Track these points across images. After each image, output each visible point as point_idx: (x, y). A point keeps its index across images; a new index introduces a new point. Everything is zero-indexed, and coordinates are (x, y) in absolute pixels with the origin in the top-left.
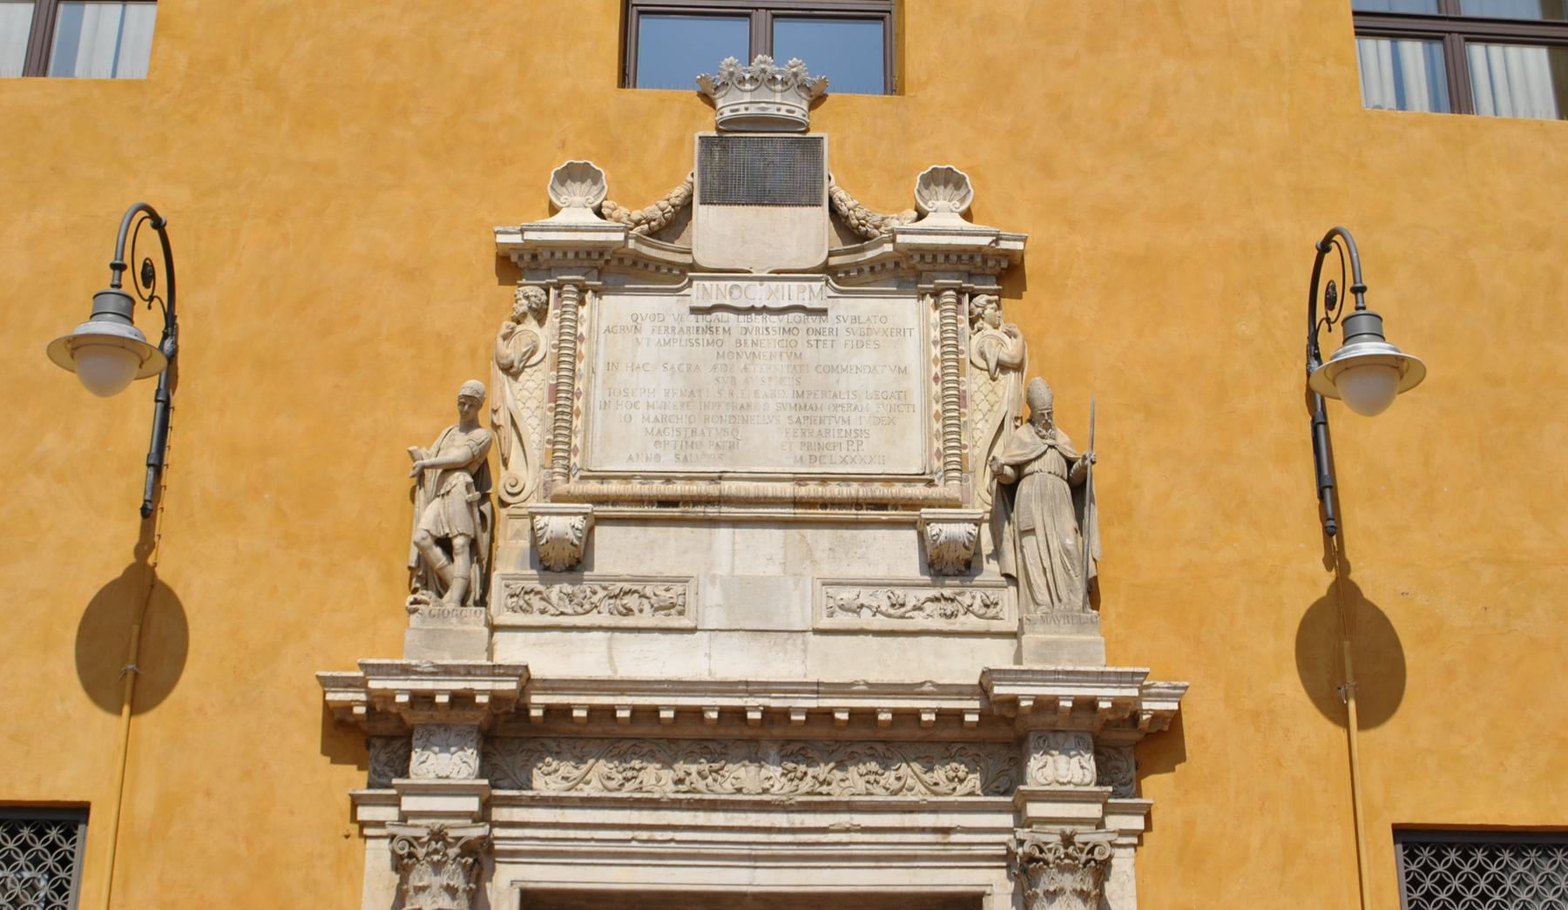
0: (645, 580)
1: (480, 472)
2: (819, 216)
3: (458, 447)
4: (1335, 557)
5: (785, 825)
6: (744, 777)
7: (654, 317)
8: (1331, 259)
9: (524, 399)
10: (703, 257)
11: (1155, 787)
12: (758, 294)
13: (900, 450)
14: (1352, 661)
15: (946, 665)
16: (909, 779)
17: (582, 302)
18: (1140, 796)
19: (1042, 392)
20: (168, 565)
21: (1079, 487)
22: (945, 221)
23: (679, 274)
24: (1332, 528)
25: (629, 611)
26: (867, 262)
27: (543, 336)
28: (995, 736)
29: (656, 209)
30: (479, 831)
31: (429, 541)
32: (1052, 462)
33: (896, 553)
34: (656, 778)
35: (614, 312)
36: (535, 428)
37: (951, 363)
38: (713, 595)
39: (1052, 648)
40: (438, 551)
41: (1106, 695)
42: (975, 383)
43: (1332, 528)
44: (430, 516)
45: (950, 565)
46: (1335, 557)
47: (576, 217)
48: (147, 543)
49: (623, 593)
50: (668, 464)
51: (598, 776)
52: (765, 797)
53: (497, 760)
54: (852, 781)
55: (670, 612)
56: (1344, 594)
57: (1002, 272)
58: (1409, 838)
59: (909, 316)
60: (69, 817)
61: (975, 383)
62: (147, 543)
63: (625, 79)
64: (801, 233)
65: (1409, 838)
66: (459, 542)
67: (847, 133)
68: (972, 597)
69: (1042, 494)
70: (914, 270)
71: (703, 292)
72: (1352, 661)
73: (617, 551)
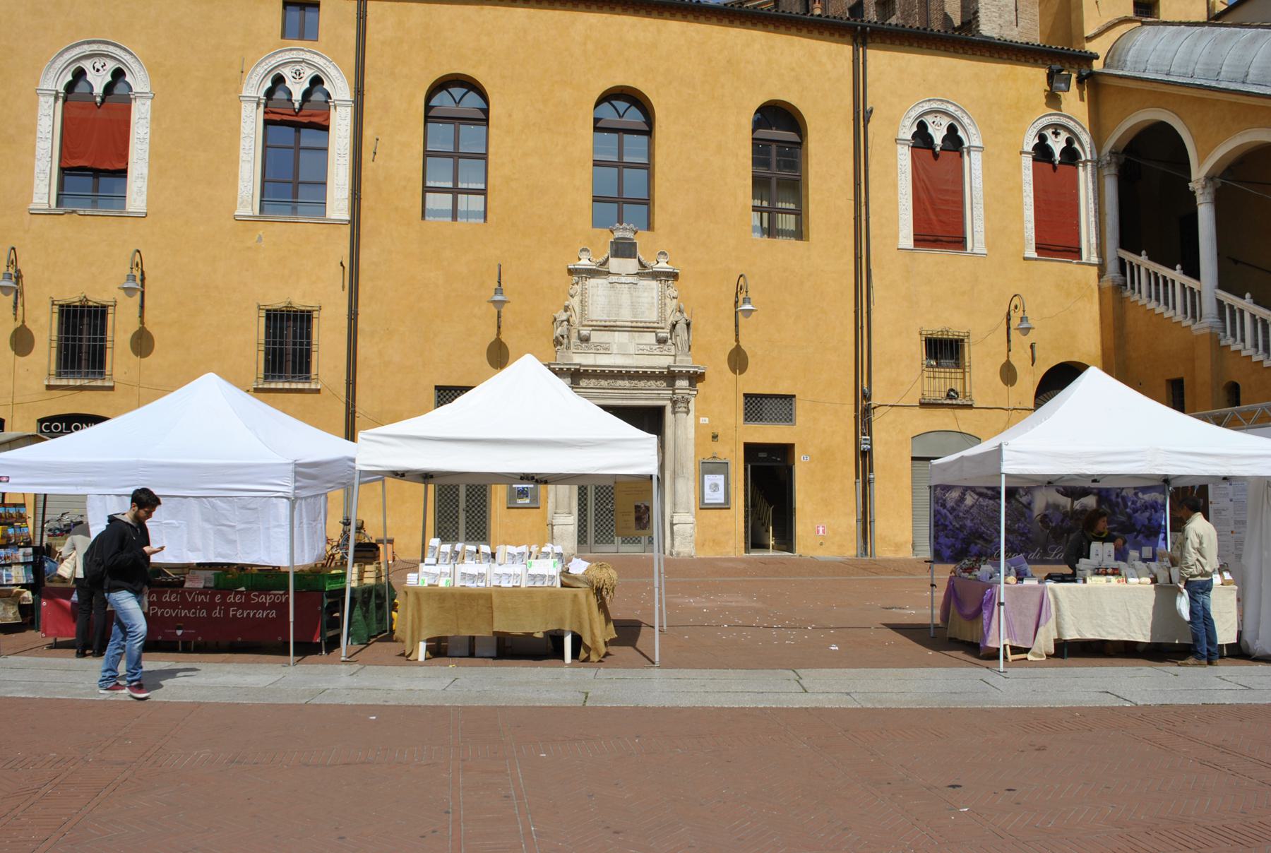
1: (568, 321)
3: (564, 317)
4: (737, 340)
6: (620, 383)
9: (575, 302)
11: (699, 385)
12: (623, 280)
13: (651, 316)
14: (738, 360)
15: (662, 361)
16: (652, 383)
19: (682, 306)
20: (504, 338)
21: (688, 325)
22: (663, 266)
24: (737, 335)
26: (645, 272)
27: (578, 288)
28: (670, 377)
29: (601, 260)
32: (683, 321)
33: (650, 338)
34: (604, 383)
35: (593, 282)
36: (577, 309)
37: (663, 297)
39: (682, 361)
41: (692, 370)
42: (668, 301)
43: (737, 335)
44: (559, 331)
45: (662, 341)
46: (737, 340)
47: (584, 262)
48: (499, 333)
49: (597, 346)
51: (593, 382)
52: (347, 265)
54: (642, 384)
55: (605, 349)
56: (738, 347)
57: (674, 276)
58: (746, 396)
59: (654, 284)
60: (791, 397)
61: (668, 301)
62: (499, 333)
64: (631, 265)
65: (746, 396)
67: (642, 240)
68: (666, 348)
69: (681, 327)
70: (656, 275)
71: (613, 279)
72: (738, 360)
73: (596, 337)
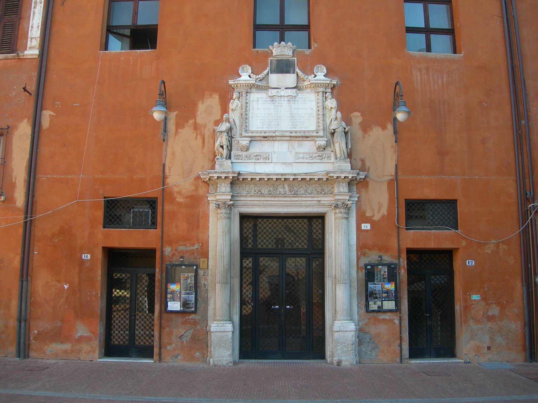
0: (261, 153)
2: (295, 76)
5: (161, 207)
7: (261, 98)
8: (397, 86)
10: (272, 85)
13: (310, 124)
17: (247, 95)
18: (453, 355)
23: (267, 88)
25: (258, 159)
30: (232, 202)
31: (219, 146)
33: (308, 147)
38: (274, 156)
40: (221, 149)
49: (257, 156)
50: (265, 129)
53: (234, 188)
63: (254, 47)
66: (225, 147)
